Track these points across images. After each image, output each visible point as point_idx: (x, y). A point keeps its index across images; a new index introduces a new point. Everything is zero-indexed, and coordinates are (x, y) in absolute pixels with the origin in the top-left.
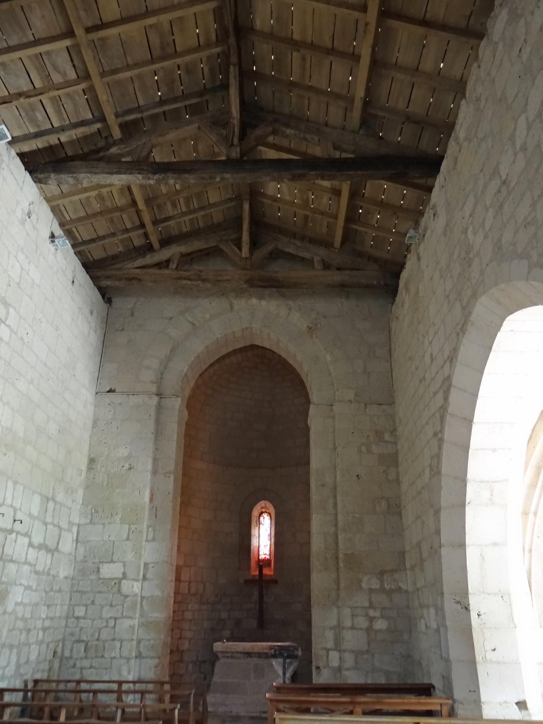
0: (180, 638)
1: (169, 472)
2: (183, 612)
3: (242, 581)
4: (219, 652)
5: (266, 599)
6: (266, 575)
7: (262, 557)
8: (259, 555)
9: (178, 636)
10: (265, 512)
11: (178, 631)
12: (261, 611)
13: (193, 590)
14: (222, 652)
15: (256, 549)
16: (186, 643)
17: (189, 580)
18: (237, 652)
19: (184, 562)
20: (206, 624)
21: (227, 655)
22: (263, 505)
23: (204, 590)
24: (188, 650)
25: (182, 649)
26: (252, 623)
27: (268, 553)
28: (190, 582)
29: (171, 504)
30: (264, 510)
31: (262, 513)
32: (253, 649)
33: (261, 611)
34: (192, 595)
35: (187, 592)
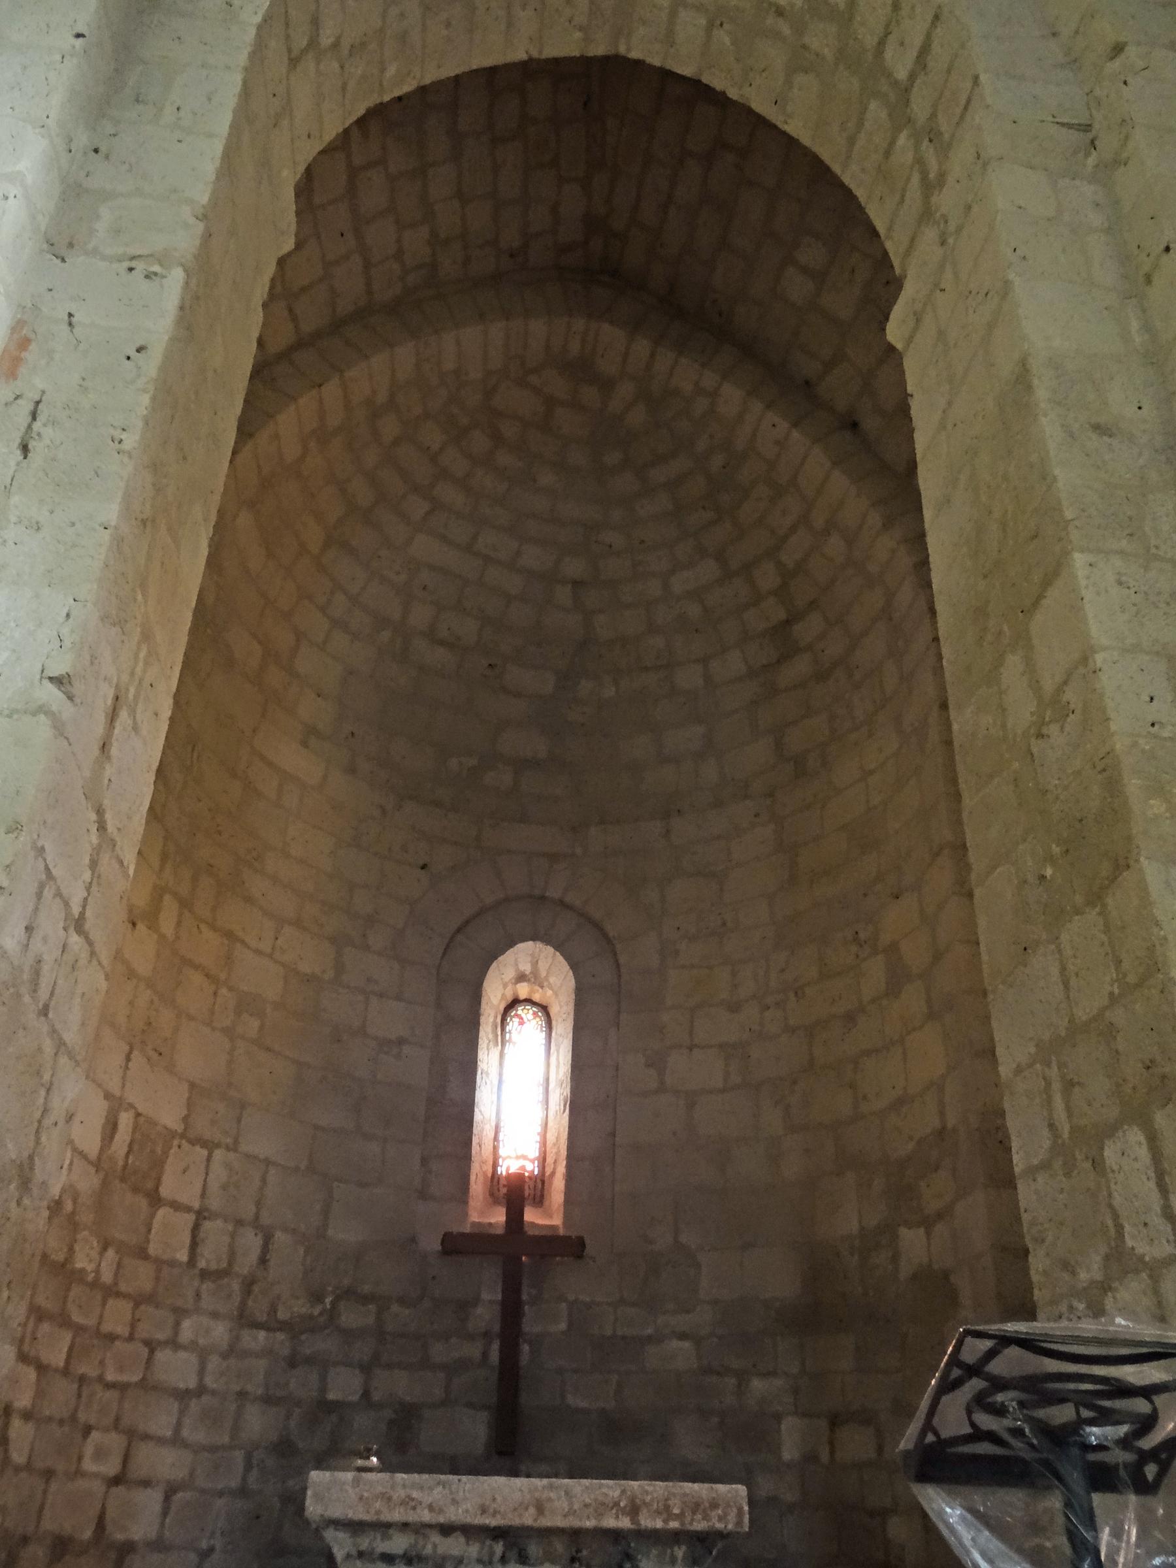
0: (116, 1481)
1: (163, 258)
2: (152, 1346)
3: (431, 1243)
4: (336, 1523)
5: (531, 1325)
6: (533, 1224)
7: (509, 1165)
8: (495, 1165)
9: (111, 1468)
10: (529, 1001)
11: (116, 1441)
12: (510, 1375)
13: (209, 1258)
14: (355, 1527)
15: (489, 1133)
16: (151, 1500)
17: (196, 1205)
18: (447, 1530)
19: (185, 1119)
20: (258, 1423)
21: (383, 1547)
22: (526, 968)
23: (263, 1261)
24: (158, 1545)
25: (120, 1536)
26: (476, 1429)
27: (534, 1152)
28: (202, 1215)
29: (146, 399)
30: (523, 990)
31: (515, 1003)
32: (540, 1509)
33: (510, 1375)
34: (205, 1275)
35: (183, 1256)
